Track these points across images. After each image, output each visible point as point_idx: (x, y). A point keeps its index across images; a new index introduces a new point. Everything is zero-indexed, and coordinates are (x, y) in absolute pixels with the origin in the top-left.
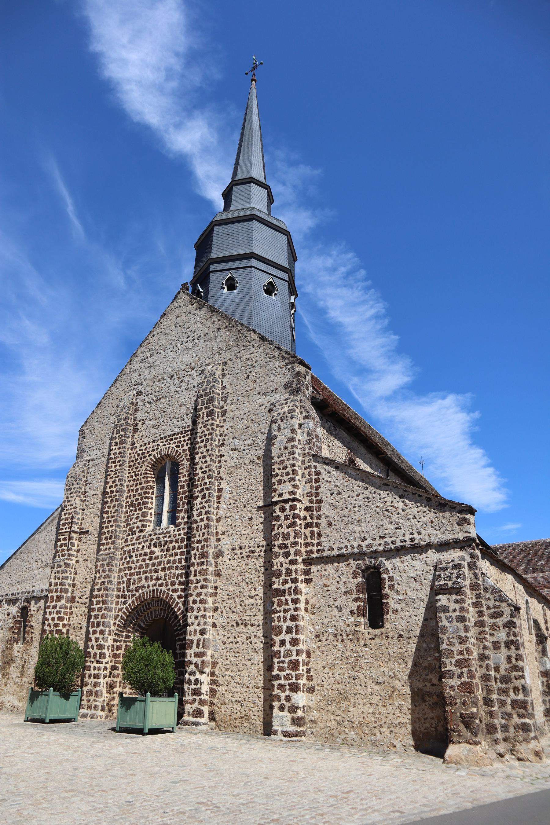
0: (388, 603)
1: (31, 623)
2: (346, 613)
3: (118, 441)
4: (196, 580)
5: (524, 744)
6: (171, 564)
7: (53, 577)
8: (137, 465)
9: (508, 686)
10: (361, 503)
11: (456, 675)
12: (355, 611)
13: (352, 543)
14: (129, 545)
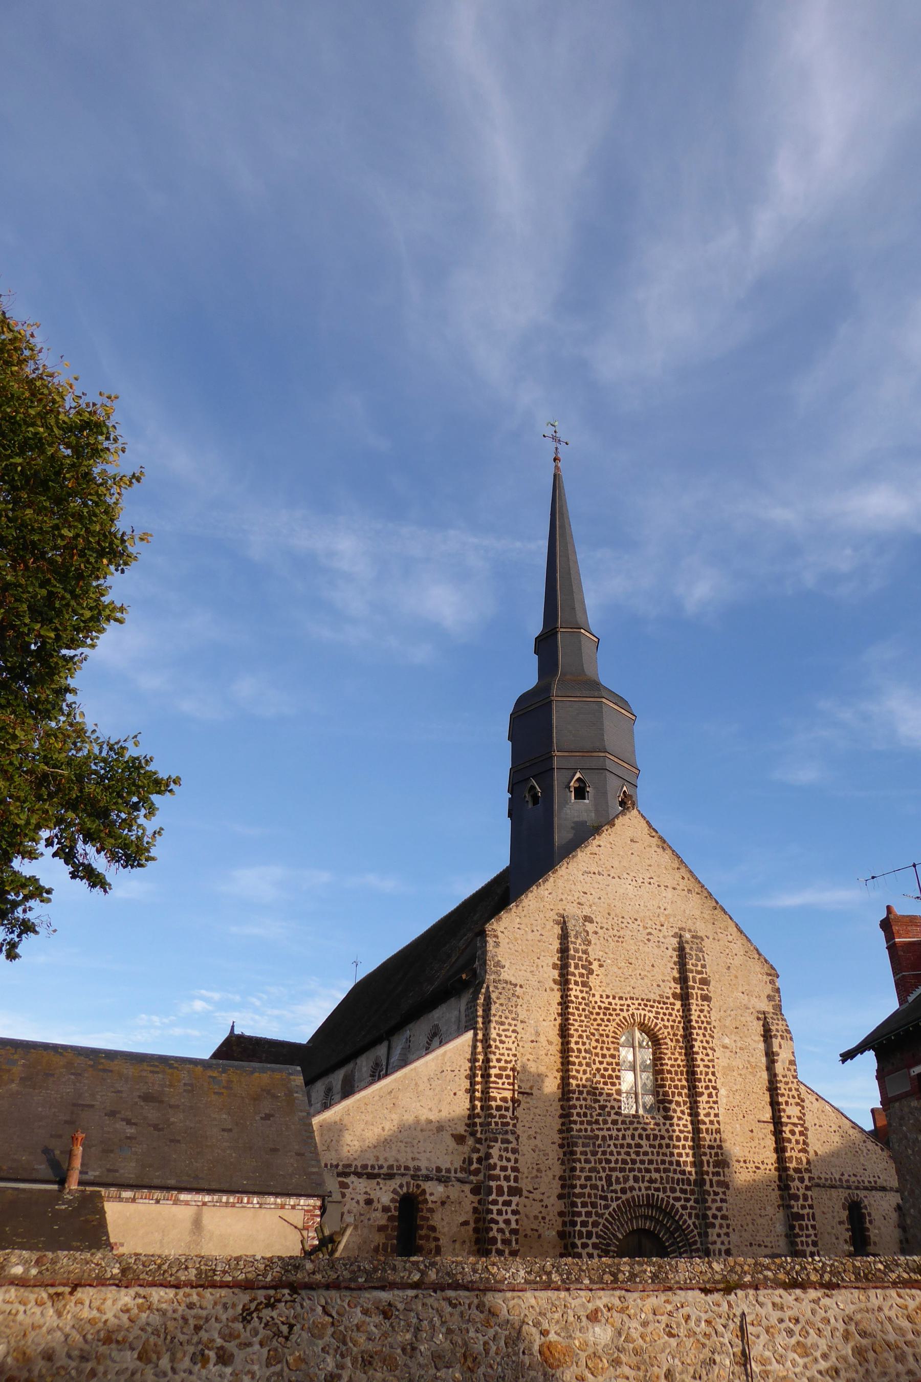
1: (431, 1223)
4: (714, 1191)
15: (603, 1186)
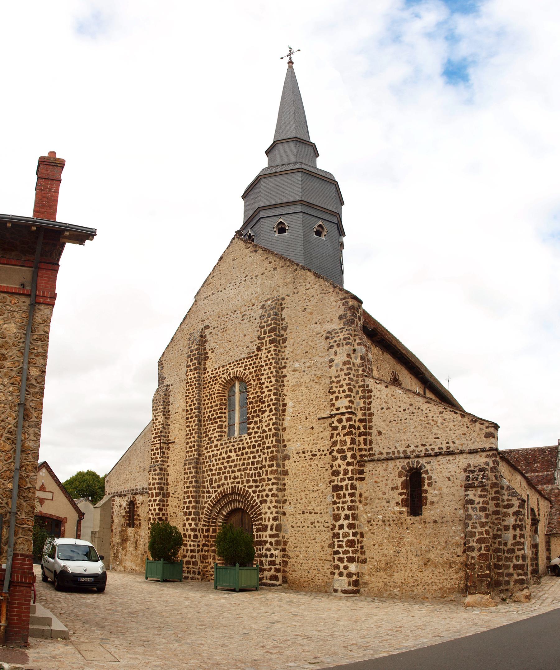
0: (426, 497)
1: (138, 513)
2: (393, 503)
3: (192, 368)
4: (268, 478)
5: (519, 592)
6: (245, 466)
7: (151, 479)
8: (210, 387)
9: (512, 555)
10: (407, 416)
11: (476, 549)
12: (400, 502)
13: (399, 449)
14: (209, 452)
15: (208, 485)
